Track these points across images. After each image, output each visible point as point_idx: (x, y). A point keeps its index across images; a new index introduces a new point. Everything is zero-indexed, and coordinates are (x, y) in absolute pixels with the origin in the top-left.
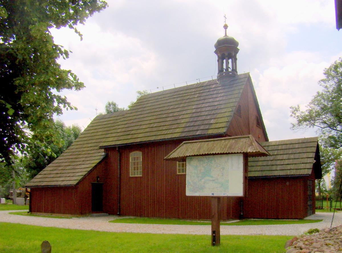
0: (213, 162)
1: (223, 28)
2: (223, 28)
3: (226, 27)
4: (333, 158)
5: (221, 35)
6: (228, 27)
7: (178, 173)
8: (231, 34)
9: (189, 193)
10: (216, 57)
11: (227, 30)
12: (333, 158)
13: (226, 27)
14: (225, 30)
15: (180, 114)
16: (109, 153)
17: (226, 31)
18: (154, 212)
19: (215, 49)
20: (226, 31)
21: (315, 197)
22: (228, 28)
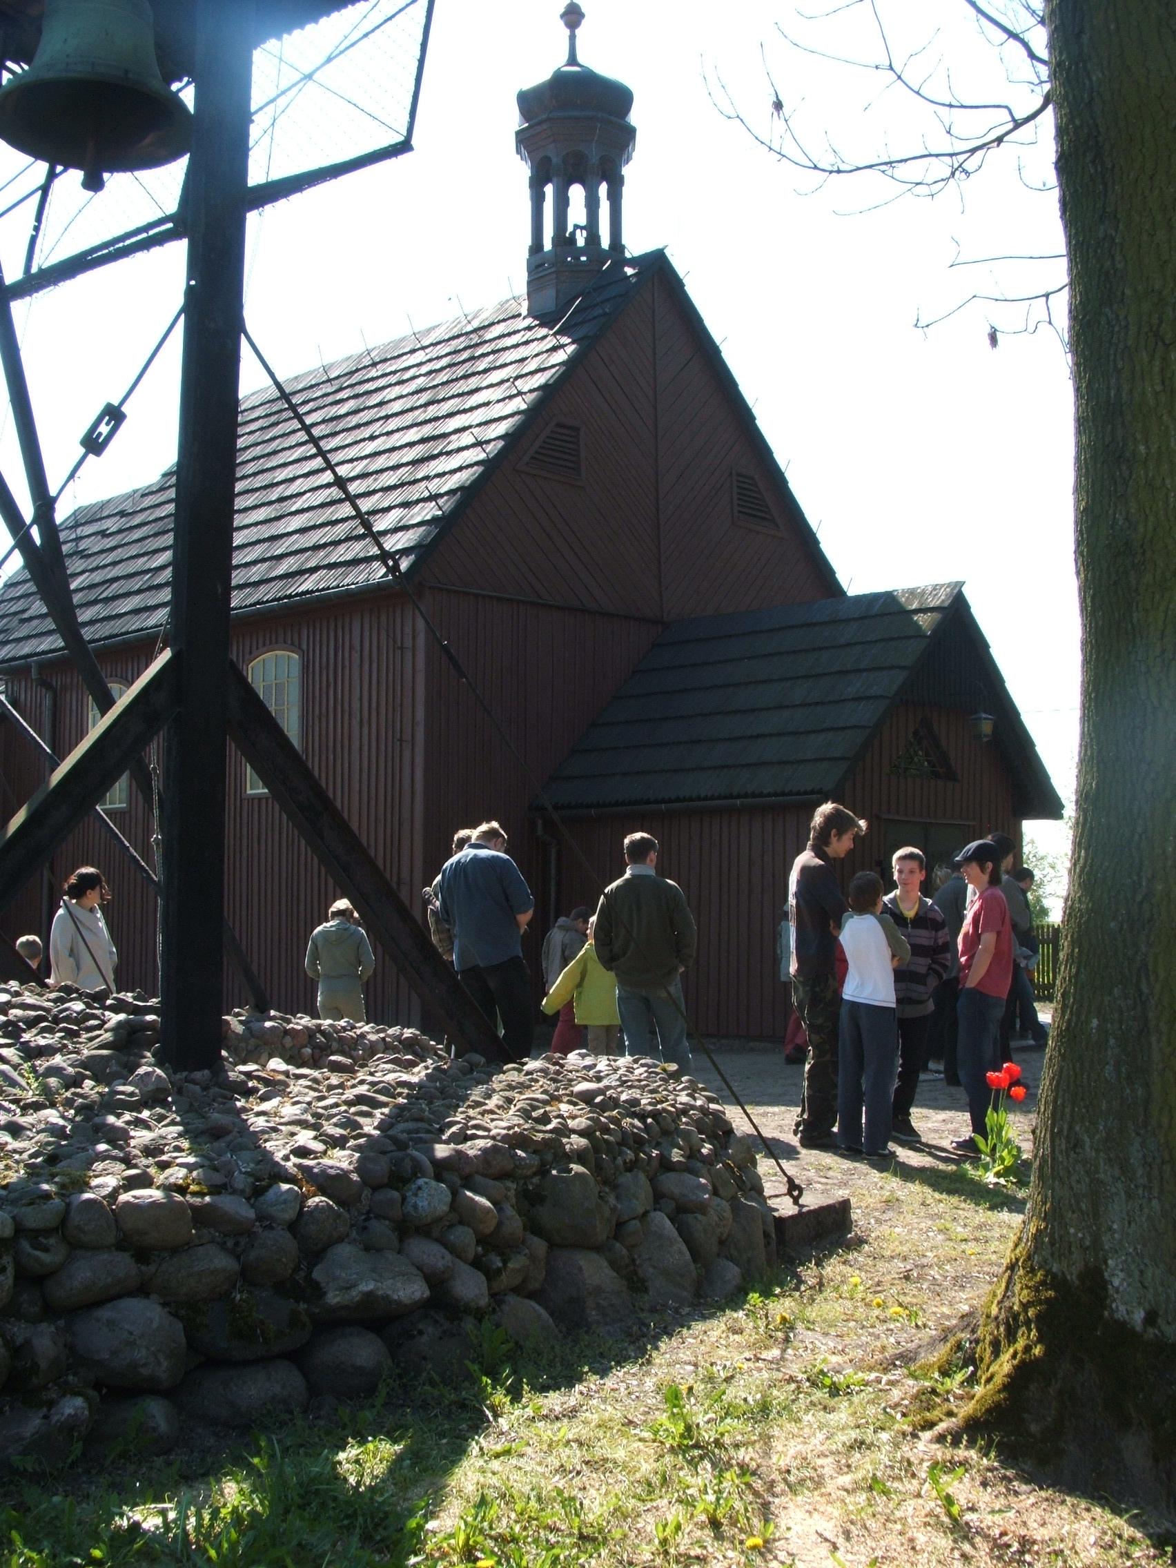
0: (1064, 1511)
1: (561, 24)
2: (561, 24)
3: (573, 17)
4: (727, 1278)
6: (582, 16)
7: (249, 792)
9: (82, 173)
10: (522, 171)
11: (577, 31)
12: (727, 1278)
13: (573, 17)
14: (567, 32)
15: (151, 603)
16: (1017, 1219)
17: (572, 38)
18: (520, 393)
20: (572, 38)
21: (441, 1477)
22: (584, 22)
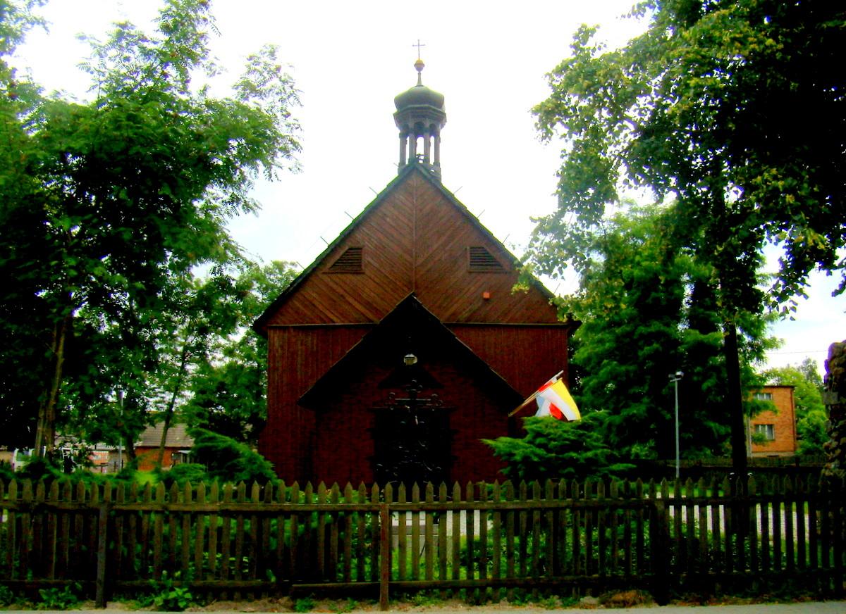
1: (414, 68)
3: (419, 66)
5: (406, 84)
8: (432, 84)
10: (396, 131)
13: (419, 66)
17: (419, 74)
19: (395, 110)
20: (419, 74)
